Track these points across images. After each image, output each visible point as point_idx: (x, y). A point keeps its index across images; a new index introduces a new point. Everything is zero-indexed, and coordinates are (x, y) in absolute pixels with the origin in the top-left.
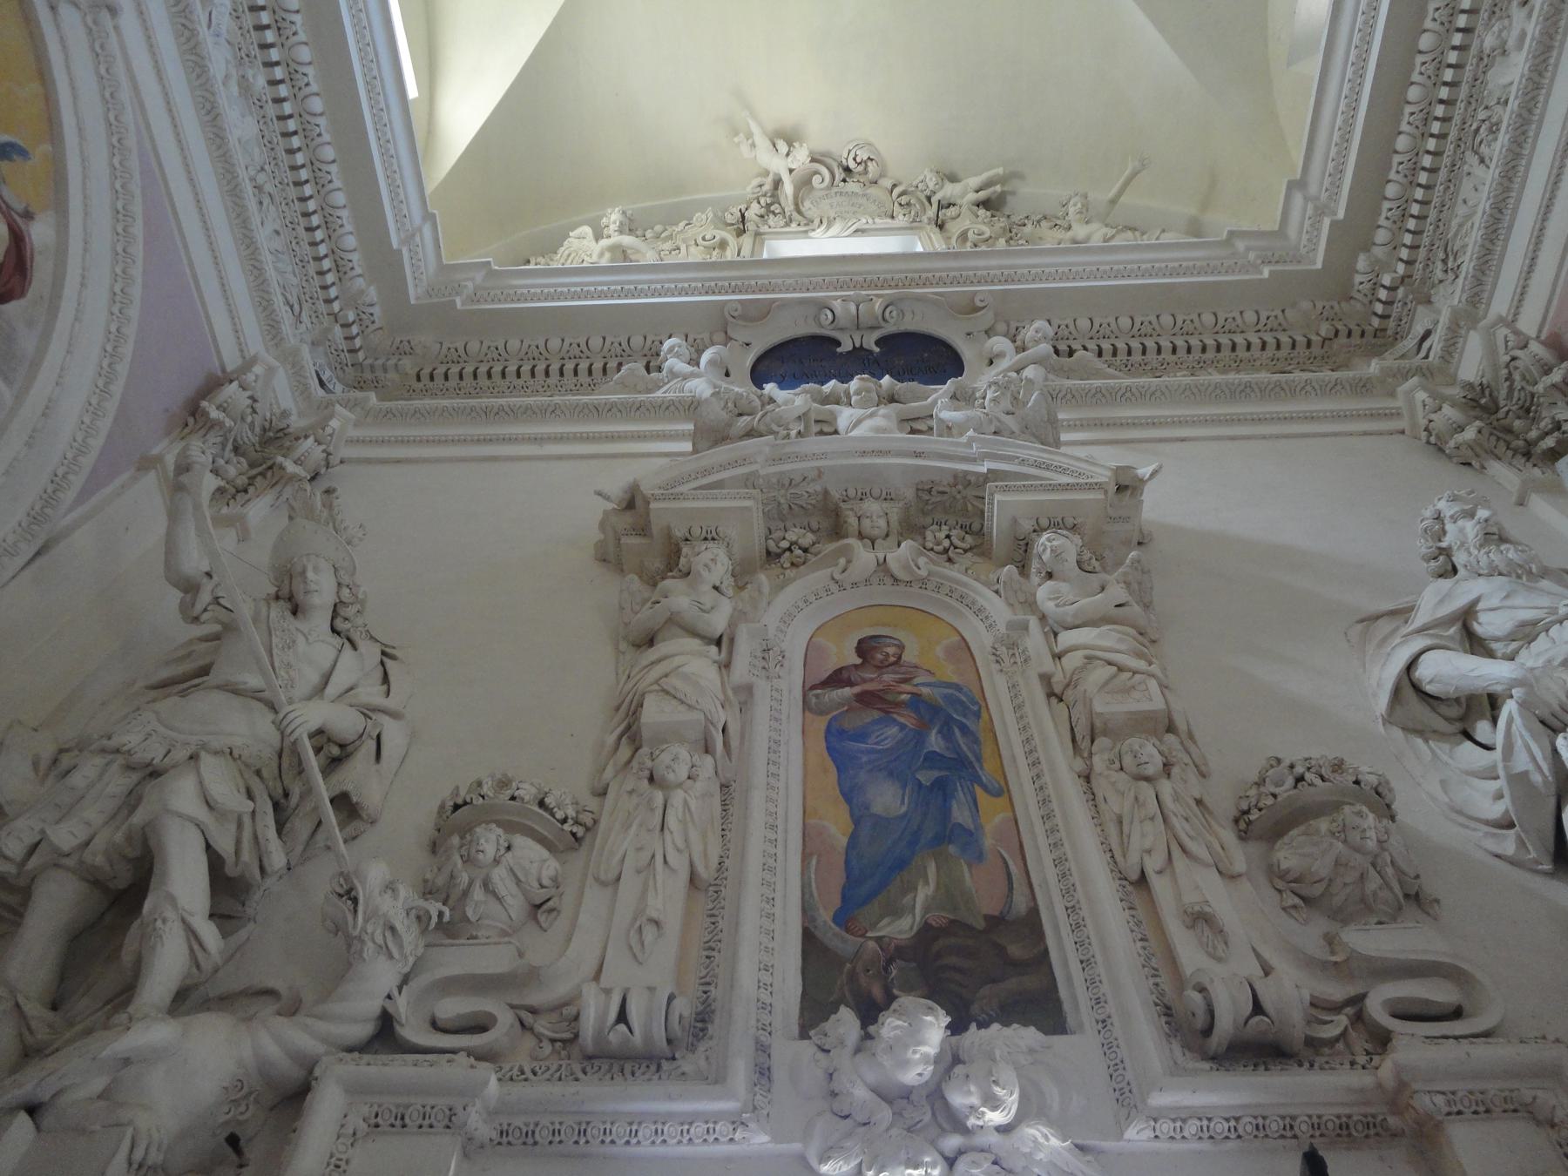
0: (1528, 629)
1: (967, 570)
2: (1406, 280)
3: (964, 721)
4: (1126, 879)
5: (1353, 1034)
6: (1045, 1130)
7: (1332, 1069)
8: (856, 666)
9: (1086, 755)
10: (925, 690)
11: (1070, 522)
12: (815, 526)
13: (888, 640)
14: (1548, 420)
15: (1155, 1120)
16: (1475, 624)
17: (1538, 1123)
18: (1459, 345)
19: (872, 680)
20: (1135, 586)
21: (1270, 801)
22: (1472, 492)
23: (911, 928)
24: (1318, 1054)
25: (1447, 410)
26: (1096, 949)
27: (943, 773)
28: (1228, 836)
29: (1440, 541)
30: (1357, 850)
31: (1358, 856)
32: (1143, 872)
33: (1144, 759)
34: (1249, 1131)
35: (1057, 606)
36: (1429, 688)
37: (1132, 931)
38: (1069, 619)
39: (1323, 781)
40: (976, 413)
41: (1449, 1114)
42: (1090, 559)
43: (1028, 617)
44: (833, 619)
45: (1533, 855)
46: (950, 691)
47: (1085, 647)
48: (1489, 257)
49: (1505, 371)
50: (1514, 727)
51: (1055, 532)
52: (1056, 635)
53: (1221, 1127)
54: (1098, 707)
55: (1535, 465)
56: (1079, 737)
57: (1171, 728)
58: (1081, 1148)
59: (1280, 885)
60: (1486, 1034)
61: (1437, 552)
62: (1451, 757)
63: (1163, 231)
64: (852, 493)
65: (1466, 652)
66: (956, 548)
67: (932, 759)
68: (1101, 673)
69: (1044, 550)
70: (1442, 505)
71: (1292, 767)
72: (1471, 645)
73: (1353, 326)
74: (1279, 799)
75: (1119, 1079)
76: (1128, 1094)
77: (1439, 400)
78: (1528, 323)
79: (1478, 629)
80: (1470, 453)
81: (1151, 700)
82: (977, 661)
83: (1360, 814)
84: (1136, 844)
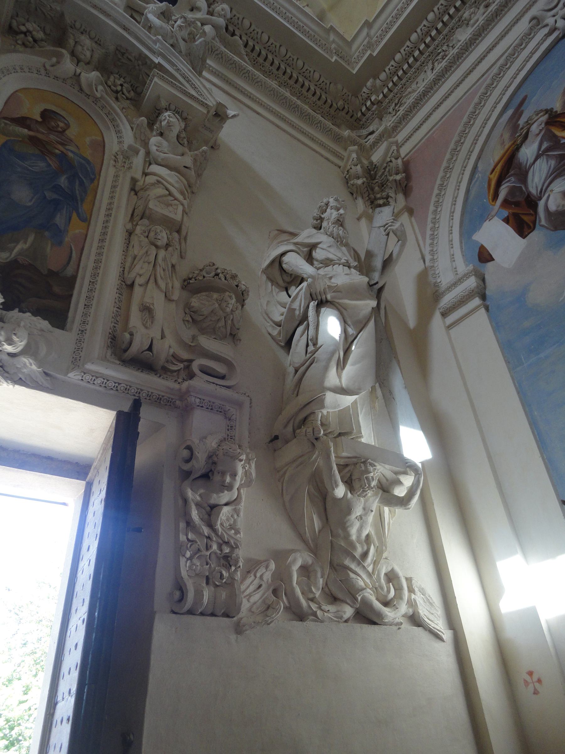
0: (328, 262)
1: (123, 108)
2: (380, 103)
3: (84, 179)
4: (124, 282)
5: (182, 371)
6: (31, 361)
7: (167, 380)
8: (37, 121)
9: (135, 223)
10: (70, 155)
11: (185, 115)
12: (48, 32)
13: (63, 119)
14: (386, 193)
15: (85, 373)
16: (314, 252)
17: (226, 418)
18: (379, 145)
19: (43, 133)
20: (198, 164)
21: (201, 278)
22: (343, 201)
23: (7, 259)
24: (165, 374)
25: (359, 167)
26: (94, 302)
27: (61, 198)
28: (177, 284)
29: (322, 214)
30: (223, 310)
31: (221, 312)
32: (133, 282)
33: (159, 237)
34: (122, 389)
35: (157, 150)
36: (284, 266)
37: (115, 303)
38: (160, 160)
39: (225, 279)
40: (168, 27)
41: (198, 406)
42: (184, 138)
43: (141, 149)
44: (36, 89)
45: (281, 338)
46: (83, 162)
47: (160, 177)
48: (409, 113)
49: (385, 165)
50: (301, 292)
51: (174, 114)
52: (150, 164)
53: (111, 384)
54: (151, 205)
55: (372, 208)
56: (135, 214)
57: (179, 231)
58: (46, 374)
59: (187, 311)
60: (228, 387)
61: (319, 217)
62: (277, 295)
63: (308, 6)
64: (78, 25)
65: (305, 260)
66: (123, 94)
67: (57, 189)
68: (160, 191)
69: (164, 120)
70: (331, 200)
71: (217, 269)
72: (308, 258)
73: (351, 111)
74: (205, 279)
75: (77, 354)
76: (78, 361)
77: (359, 161)
78: (404, 151)
79: (314, 254)
80: (355, 190)
81: (176, 214)
82: (106, 155)
83: (230, 297)
84: (137, 269)
